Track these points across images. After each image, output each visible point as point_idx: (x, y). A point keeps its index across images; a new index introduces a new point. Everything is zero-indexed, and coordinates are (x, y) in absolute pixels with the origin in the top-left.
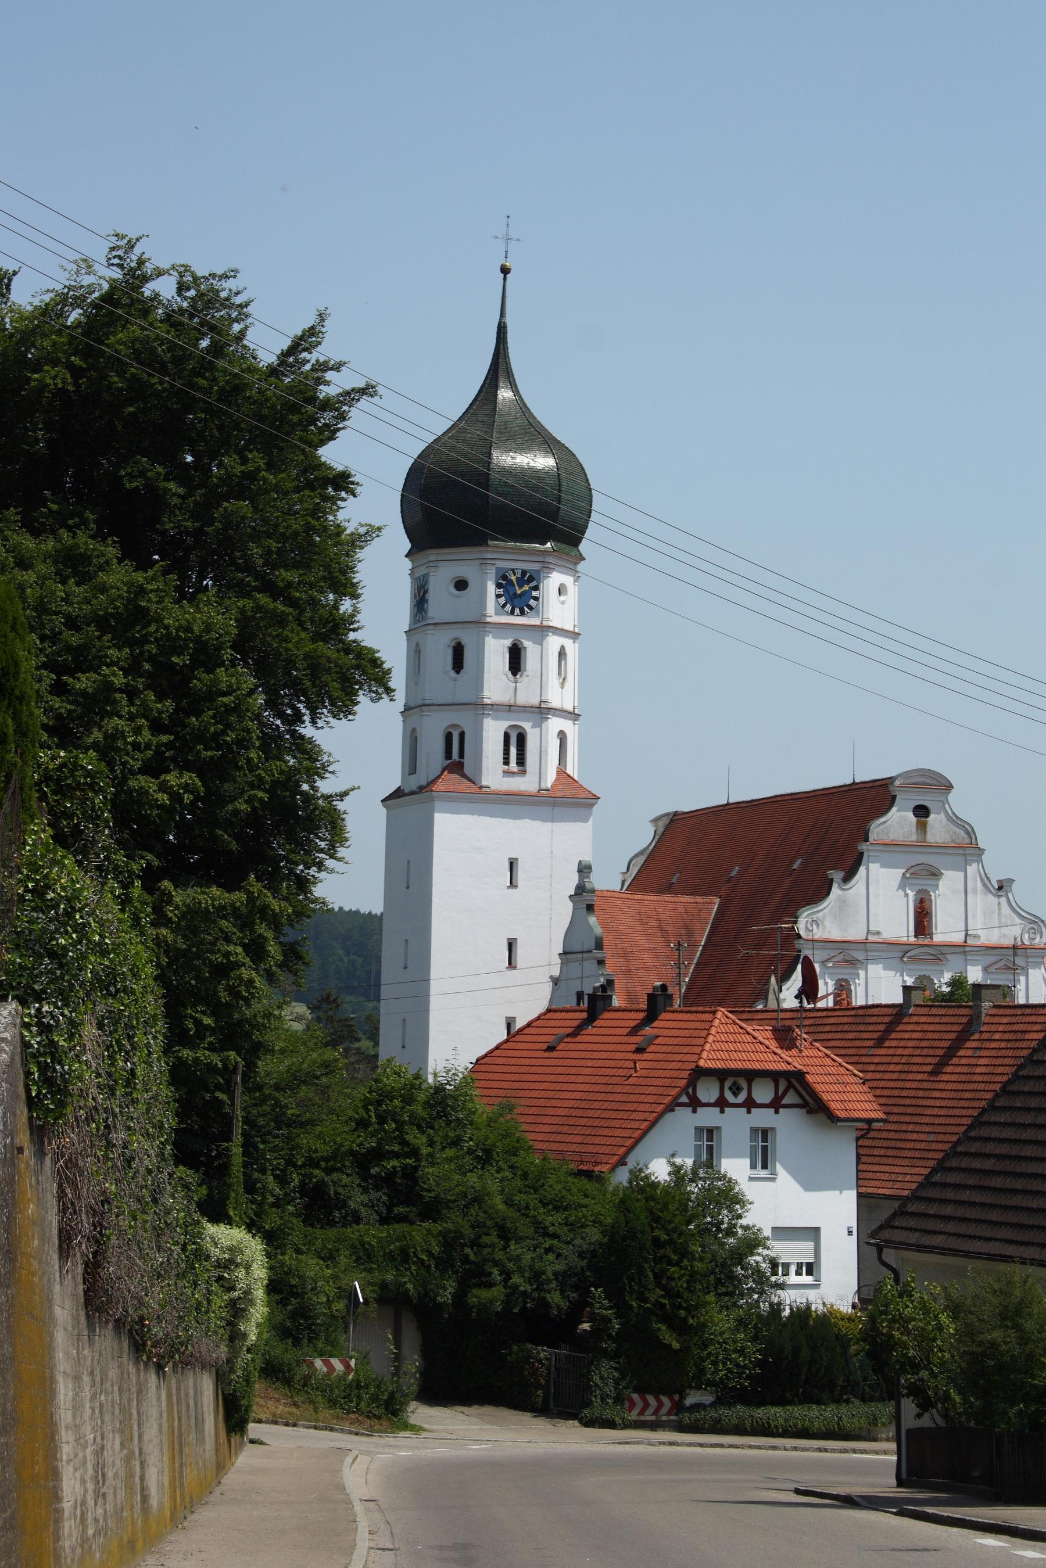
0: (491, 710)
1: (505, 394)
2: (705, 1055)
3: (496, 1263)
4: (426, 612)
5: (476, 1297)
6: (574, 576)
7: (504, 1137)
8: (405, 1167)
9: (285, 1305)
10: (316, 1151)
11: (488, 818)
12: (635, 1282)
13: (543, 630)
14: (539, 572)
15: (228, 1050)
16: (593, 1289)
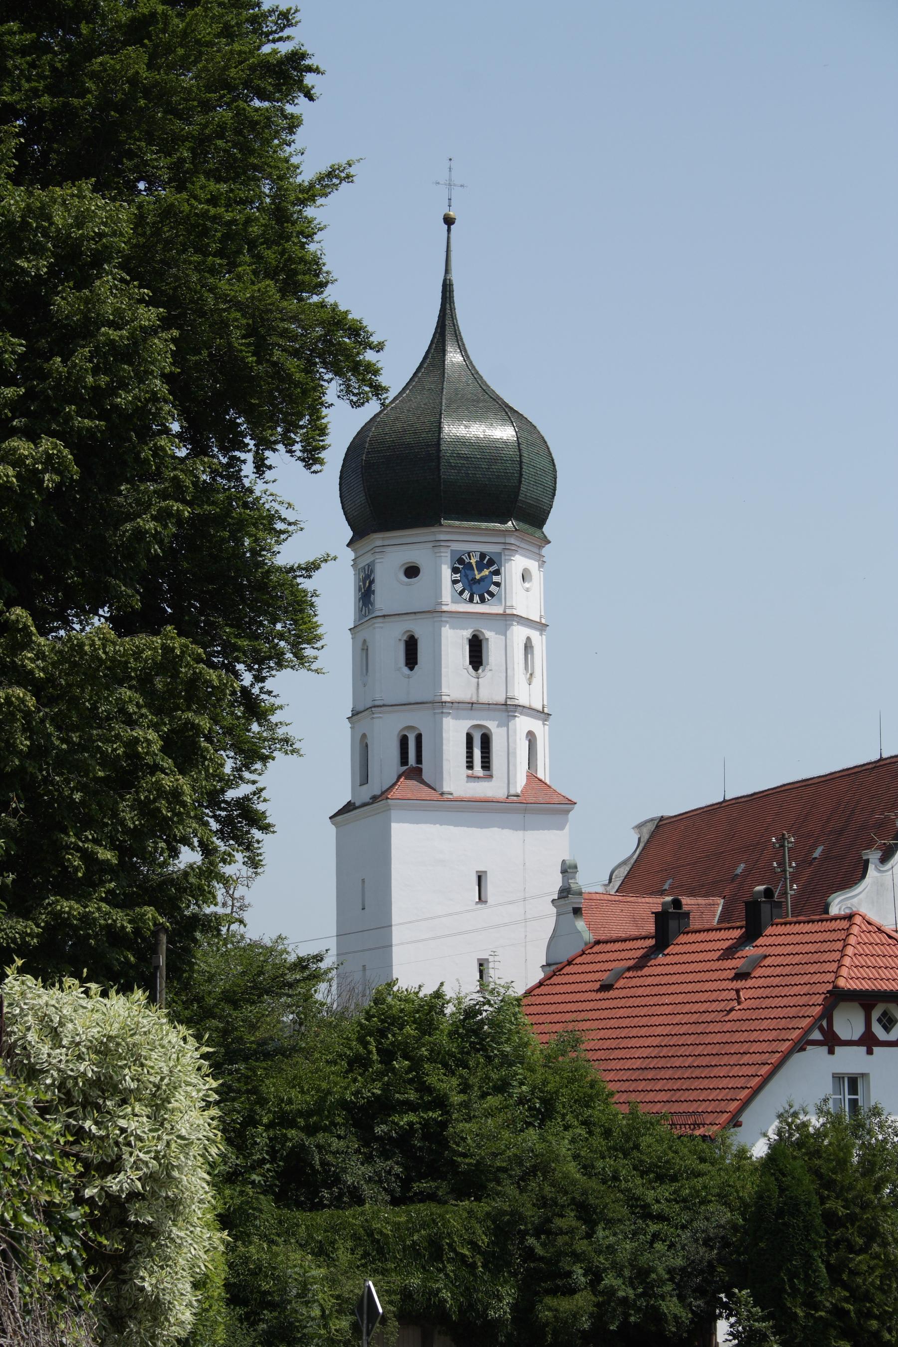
0: (451, 708)
1: (453, 357)
2: (844, 971)
3: (577, 1257)
4: (372, 604)
5: (550, 1309)
6: (538, 561)
7: (571, 1081)
8: (426, 1124)
9: (253, 1324)
10: (290, 1102)
11: (451, 828)
12: (798, 1278)
13: (507, 619)
14: (500, 554)
15: (140, 905)
16: (736, 1291)
